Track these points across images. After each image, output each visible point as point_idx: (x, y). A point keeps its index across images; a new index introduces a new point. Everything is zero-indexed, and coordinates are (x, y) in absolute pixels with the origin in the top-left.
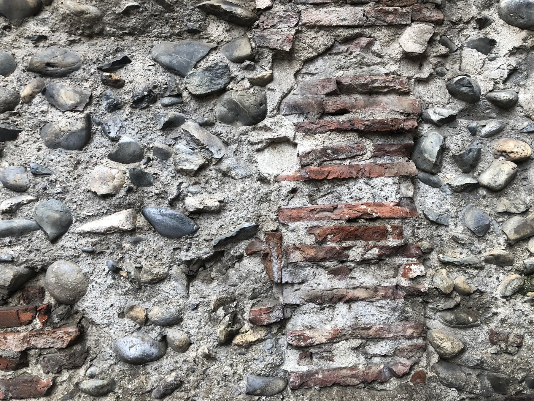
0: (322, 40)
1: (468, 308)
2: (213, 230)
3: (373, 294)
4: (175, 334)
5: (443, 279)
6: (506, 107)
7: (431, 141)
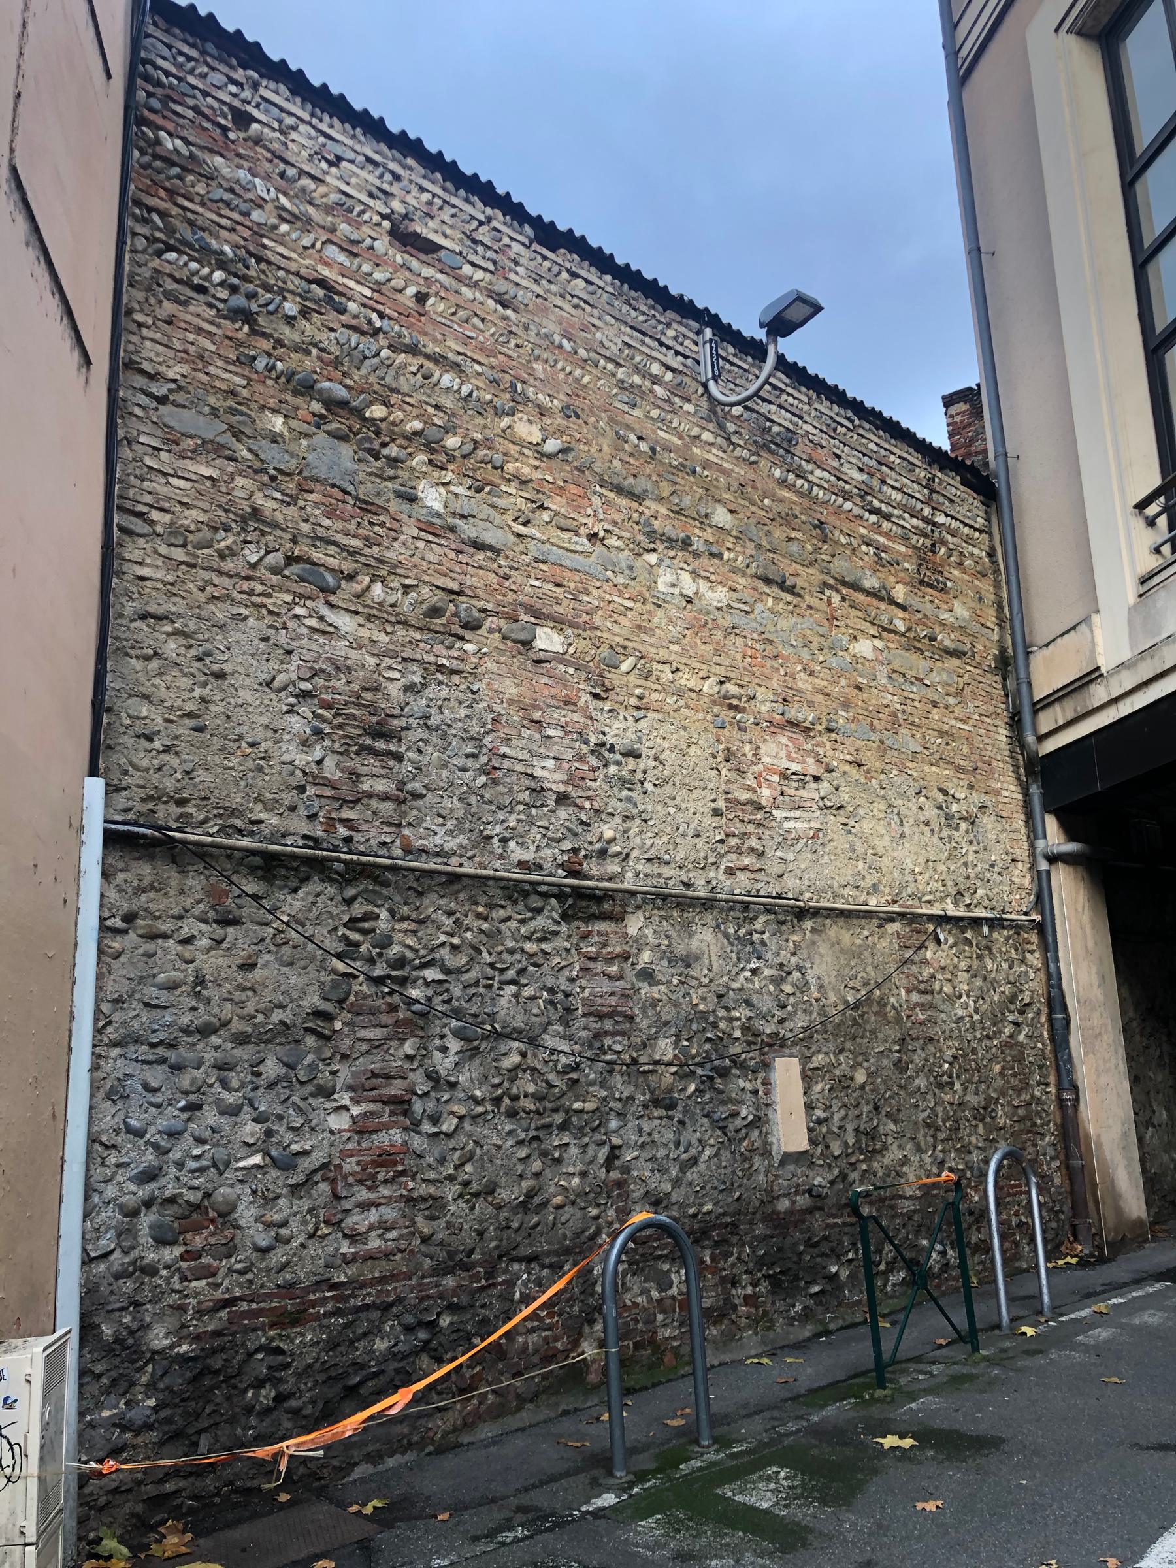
0: (364, 1047)
1: (435, 1206)
2: (305, 1164)
3: (389, 1201)
4: (284, 1232)
5: (424, 1190)
6: (453, 1085)
7: (418, 1107)
